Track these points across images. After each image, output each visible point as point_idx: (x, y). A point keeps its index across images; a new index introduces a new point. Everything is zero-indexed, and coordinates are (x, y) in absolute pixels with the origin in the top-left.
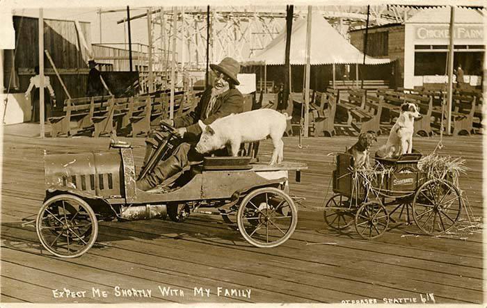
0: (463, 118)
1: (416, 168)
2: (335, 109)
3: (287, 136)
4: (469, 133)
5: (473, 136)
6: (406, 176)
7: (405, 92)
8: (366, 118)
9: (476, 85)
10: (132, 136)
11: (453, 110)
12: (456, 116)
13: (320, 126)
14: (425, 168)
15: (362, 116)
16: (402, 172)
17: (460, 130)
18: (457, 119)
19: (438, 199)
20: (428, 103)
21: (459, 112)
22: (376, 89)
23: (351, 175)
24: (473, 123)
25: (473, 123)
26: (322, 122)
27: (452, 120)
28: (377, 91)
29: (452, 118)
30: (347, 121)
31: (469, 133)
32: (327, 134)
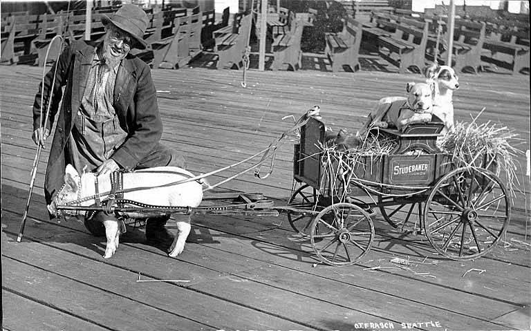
0: (468, 50)
1: (434, 146)
2: (361, 36)
3: (293, 70)
4: (476, 70)
5: (480, 75)
6: (416, 160)
7: (413, 15)
8: (407, 48)
9: (497, 9)
10: (37, 65)
11: (456, 38)
12: (458, 48)
13: (279, 56)
14: (450, 145)
15: (402, 47)
16: (410, 153)
17: (464, 65)
18: (460, 51)
19: (222, 287)
20: (479, 30)
21: (465, 42)
22: (369, 11)
23: (321, 155)
24: (482, 56)
25: (482, 56)
26: (410, 54)
27: (454, 53)
28: (370, 13)
29: (454, 49)
30: (323, 51)
31: (476, 70)
32: (347, 68)
